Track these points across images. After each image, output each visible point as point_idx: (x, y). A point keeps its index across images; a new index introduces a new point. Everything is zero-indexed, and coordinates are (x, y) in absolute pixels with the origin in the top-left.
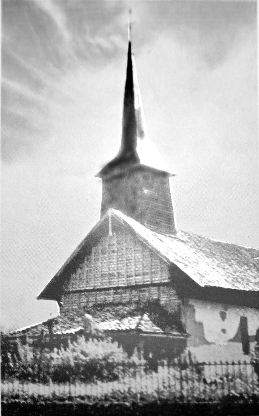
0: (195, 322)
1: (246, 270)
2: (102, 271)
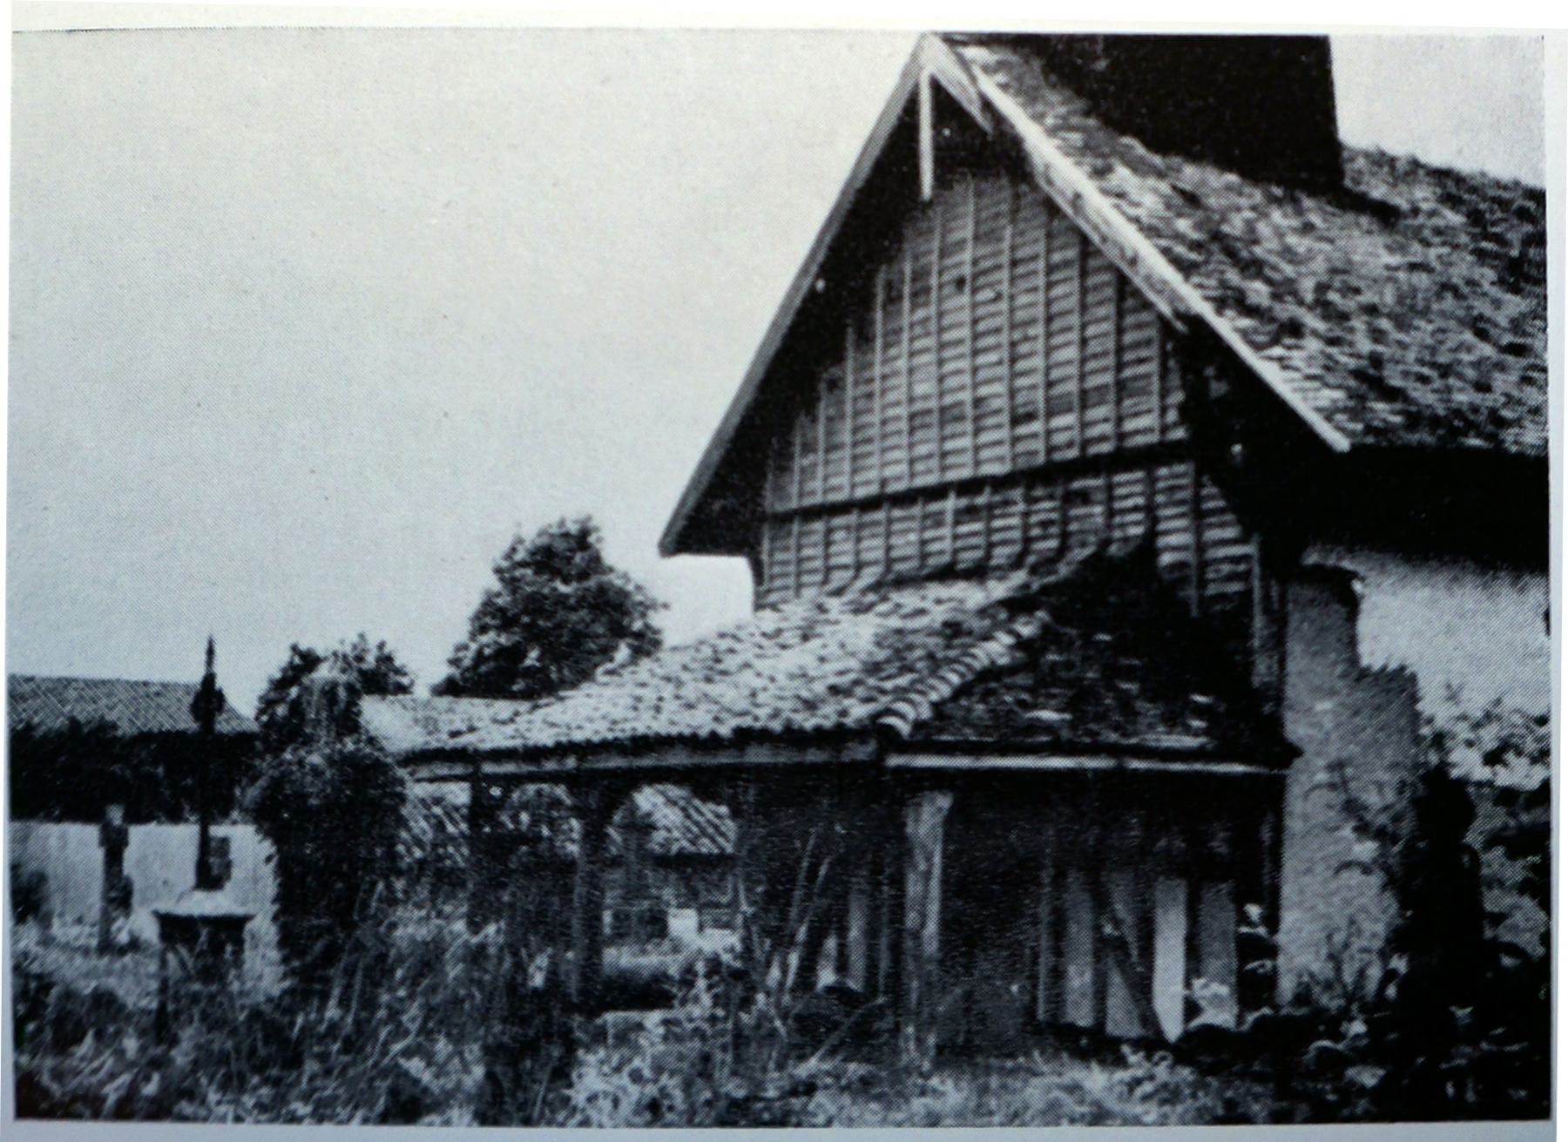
0: (1360, 675)
1: (1317, 390)
2: (911, 400)
